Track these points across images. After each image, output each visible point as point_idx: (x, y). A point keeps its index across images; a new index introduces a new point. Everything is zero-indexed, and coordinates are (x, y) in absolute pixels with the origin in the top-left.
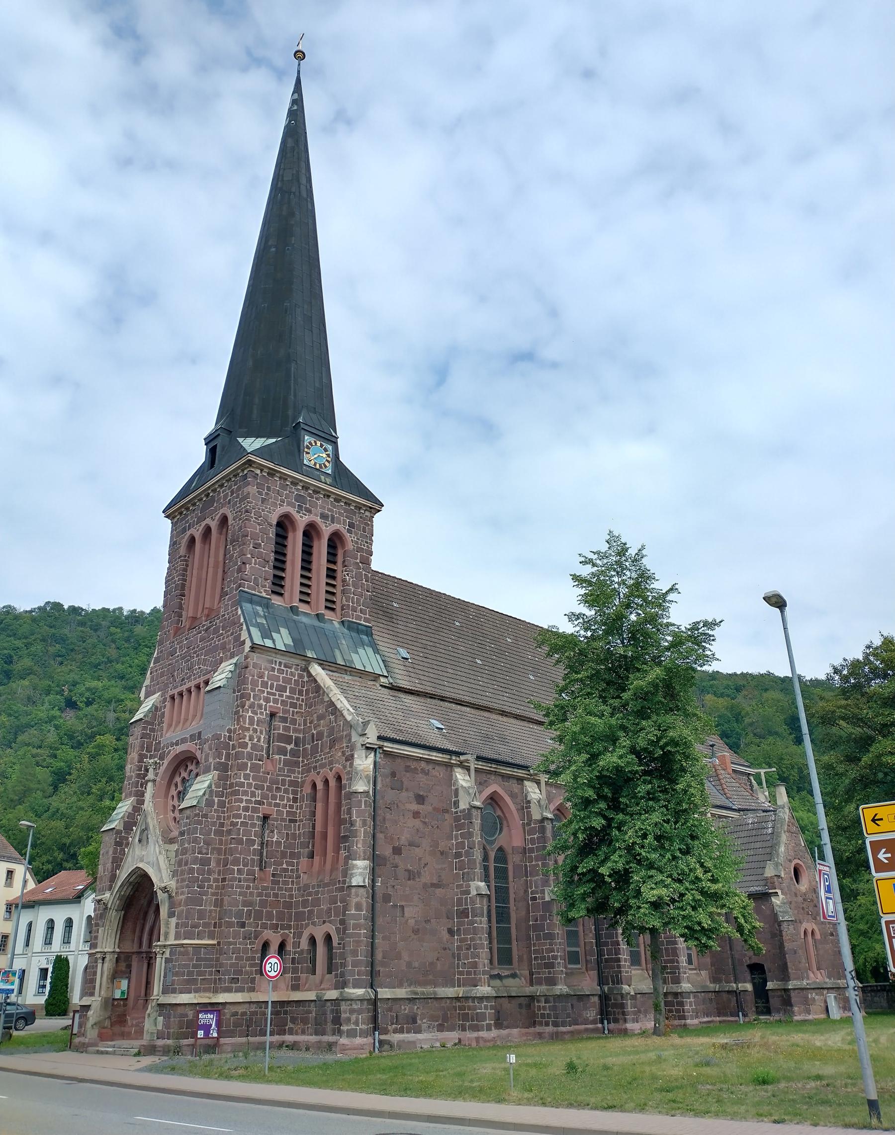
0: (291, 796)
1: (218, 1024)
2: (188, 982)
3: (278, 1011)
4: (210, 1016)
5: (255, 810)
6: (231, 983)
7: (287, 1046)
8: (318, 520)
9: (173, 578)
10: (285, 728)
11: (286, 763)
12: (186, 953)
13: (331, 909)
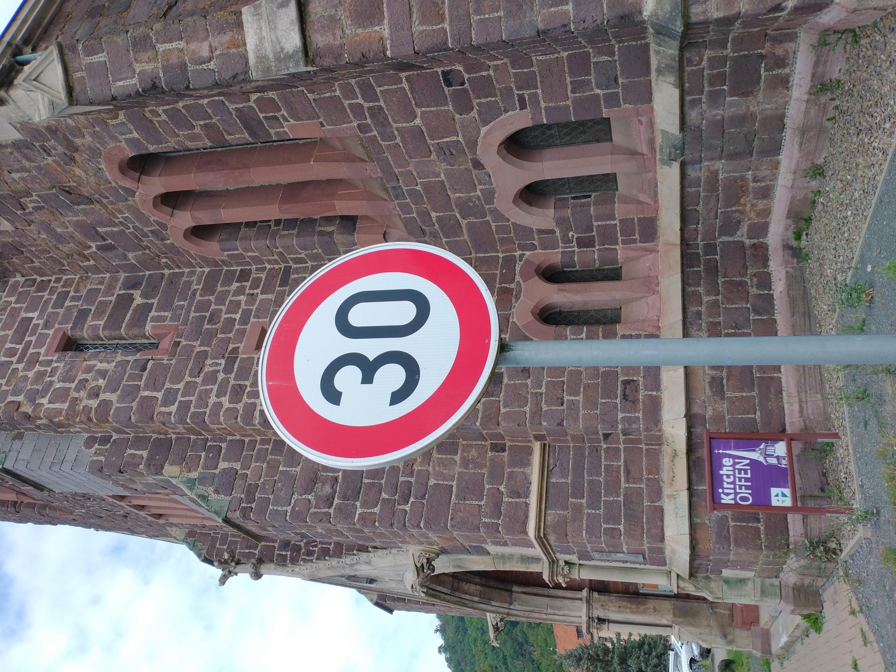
1: (749, 438)
2: (633, 517)
3: (707, 270)
4: (726, 468)
6: (635, 402)
7: (798, 237)
10: (98, 315)
12: (561, 528)
13: (440, 148)
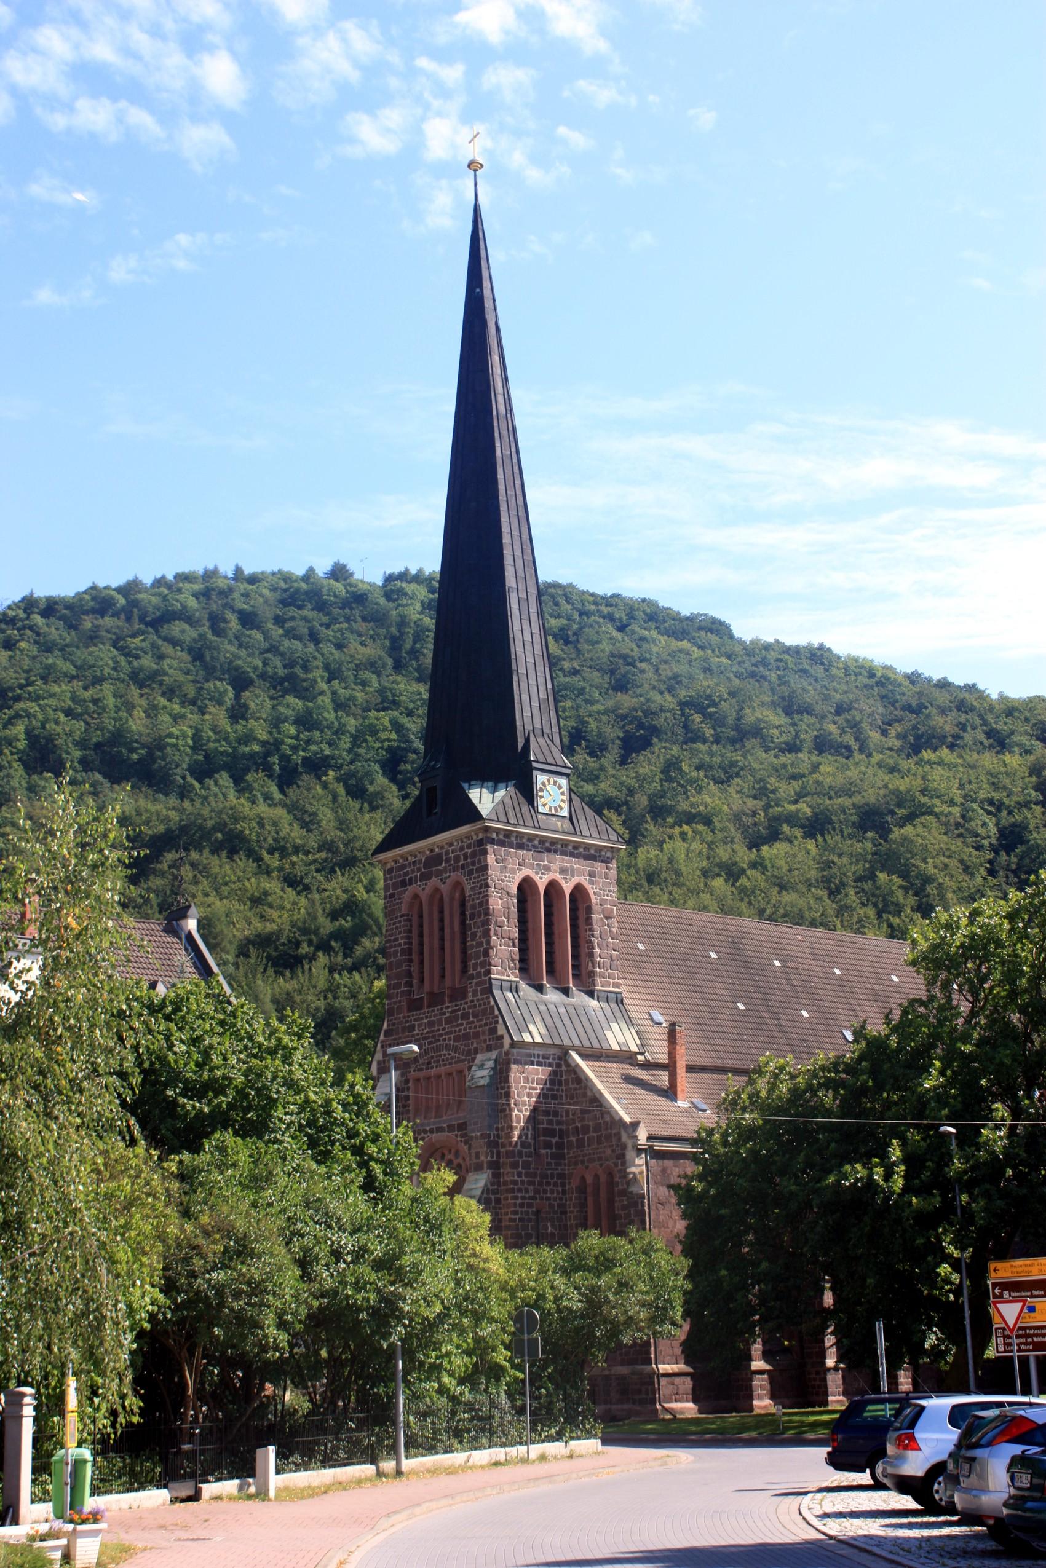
0: (560, 1189)
5: (530, 1206)
8: (558, 877)
9: (396, 940)
11: (553, 1156)
